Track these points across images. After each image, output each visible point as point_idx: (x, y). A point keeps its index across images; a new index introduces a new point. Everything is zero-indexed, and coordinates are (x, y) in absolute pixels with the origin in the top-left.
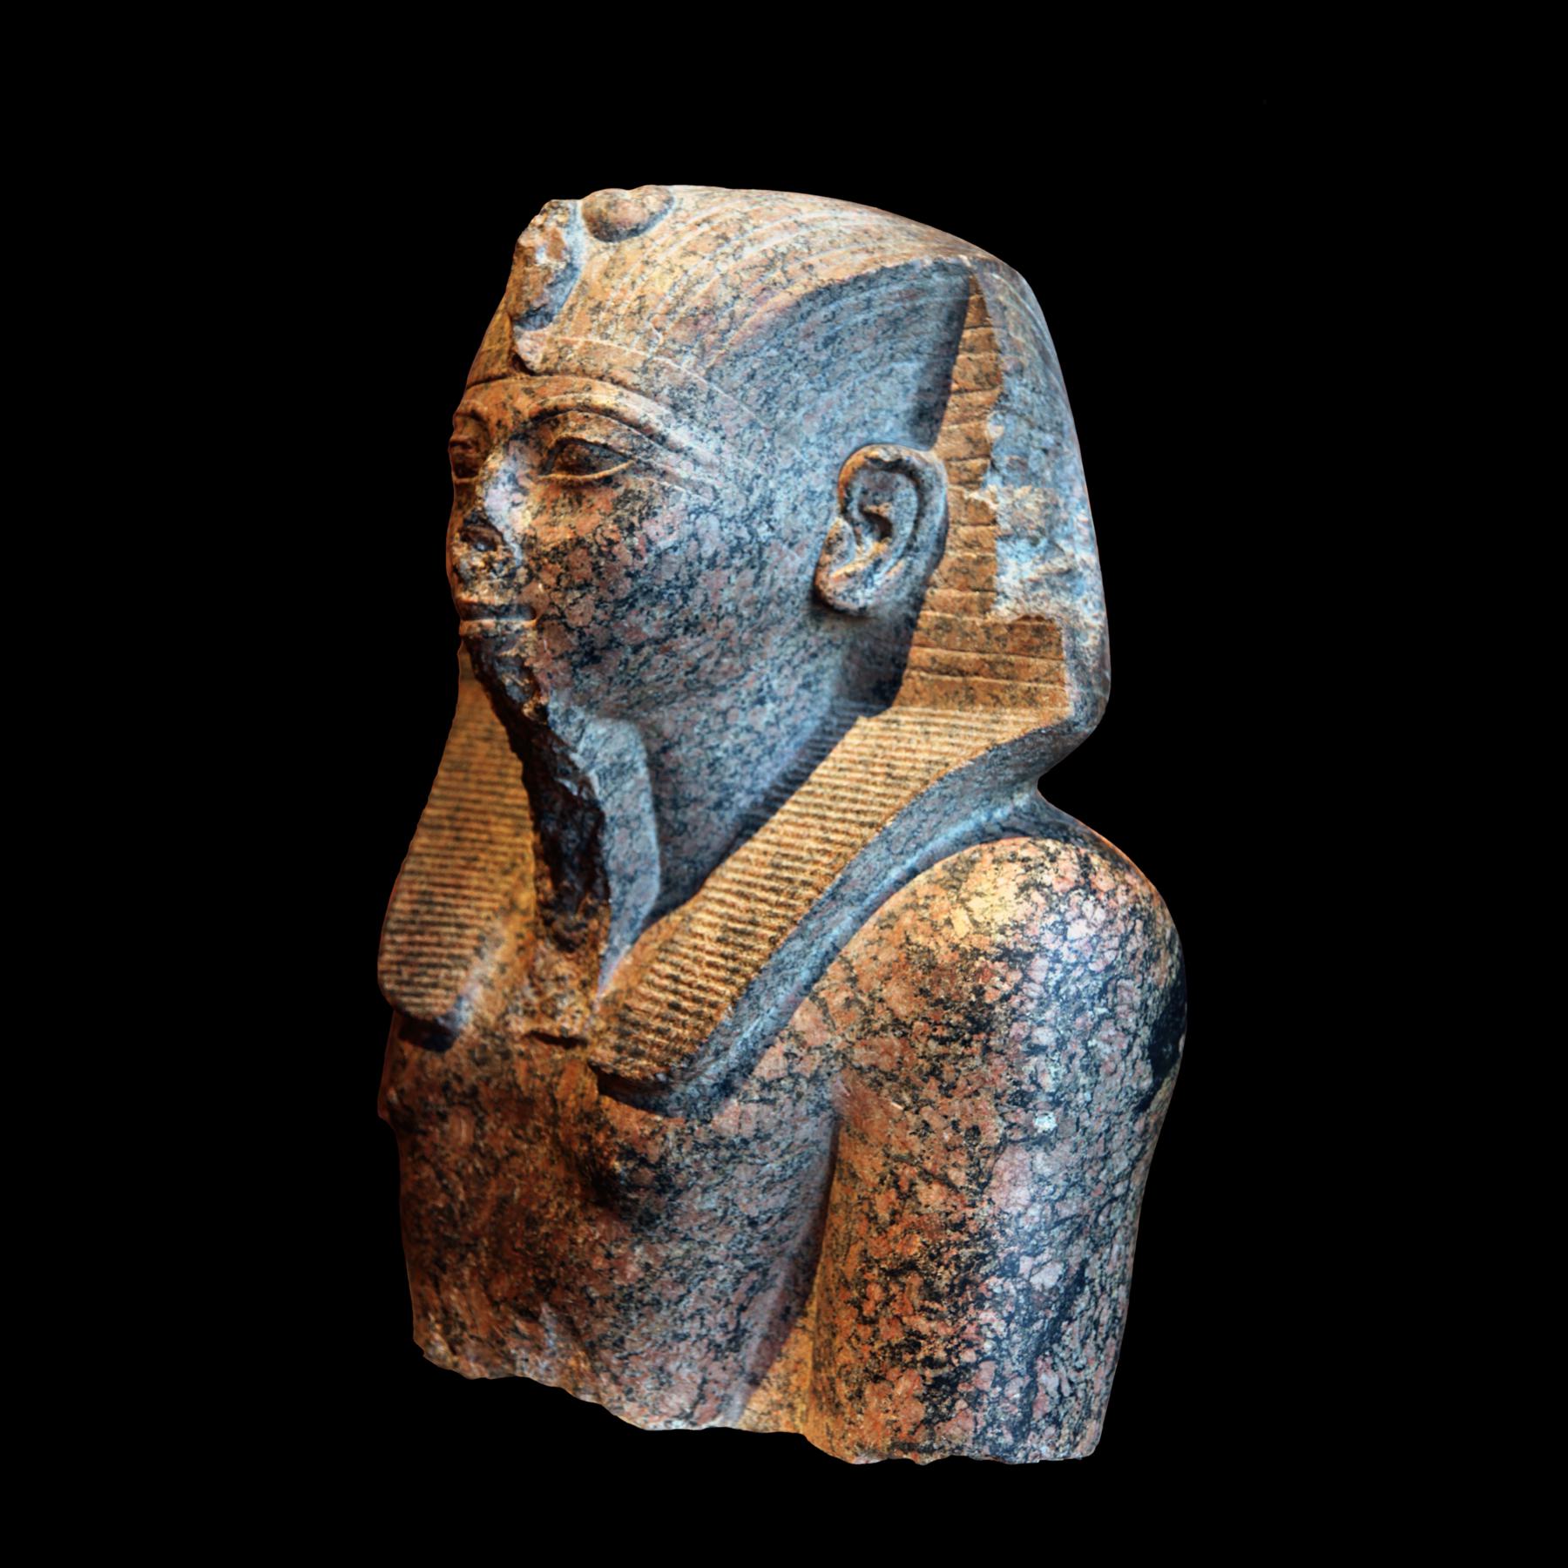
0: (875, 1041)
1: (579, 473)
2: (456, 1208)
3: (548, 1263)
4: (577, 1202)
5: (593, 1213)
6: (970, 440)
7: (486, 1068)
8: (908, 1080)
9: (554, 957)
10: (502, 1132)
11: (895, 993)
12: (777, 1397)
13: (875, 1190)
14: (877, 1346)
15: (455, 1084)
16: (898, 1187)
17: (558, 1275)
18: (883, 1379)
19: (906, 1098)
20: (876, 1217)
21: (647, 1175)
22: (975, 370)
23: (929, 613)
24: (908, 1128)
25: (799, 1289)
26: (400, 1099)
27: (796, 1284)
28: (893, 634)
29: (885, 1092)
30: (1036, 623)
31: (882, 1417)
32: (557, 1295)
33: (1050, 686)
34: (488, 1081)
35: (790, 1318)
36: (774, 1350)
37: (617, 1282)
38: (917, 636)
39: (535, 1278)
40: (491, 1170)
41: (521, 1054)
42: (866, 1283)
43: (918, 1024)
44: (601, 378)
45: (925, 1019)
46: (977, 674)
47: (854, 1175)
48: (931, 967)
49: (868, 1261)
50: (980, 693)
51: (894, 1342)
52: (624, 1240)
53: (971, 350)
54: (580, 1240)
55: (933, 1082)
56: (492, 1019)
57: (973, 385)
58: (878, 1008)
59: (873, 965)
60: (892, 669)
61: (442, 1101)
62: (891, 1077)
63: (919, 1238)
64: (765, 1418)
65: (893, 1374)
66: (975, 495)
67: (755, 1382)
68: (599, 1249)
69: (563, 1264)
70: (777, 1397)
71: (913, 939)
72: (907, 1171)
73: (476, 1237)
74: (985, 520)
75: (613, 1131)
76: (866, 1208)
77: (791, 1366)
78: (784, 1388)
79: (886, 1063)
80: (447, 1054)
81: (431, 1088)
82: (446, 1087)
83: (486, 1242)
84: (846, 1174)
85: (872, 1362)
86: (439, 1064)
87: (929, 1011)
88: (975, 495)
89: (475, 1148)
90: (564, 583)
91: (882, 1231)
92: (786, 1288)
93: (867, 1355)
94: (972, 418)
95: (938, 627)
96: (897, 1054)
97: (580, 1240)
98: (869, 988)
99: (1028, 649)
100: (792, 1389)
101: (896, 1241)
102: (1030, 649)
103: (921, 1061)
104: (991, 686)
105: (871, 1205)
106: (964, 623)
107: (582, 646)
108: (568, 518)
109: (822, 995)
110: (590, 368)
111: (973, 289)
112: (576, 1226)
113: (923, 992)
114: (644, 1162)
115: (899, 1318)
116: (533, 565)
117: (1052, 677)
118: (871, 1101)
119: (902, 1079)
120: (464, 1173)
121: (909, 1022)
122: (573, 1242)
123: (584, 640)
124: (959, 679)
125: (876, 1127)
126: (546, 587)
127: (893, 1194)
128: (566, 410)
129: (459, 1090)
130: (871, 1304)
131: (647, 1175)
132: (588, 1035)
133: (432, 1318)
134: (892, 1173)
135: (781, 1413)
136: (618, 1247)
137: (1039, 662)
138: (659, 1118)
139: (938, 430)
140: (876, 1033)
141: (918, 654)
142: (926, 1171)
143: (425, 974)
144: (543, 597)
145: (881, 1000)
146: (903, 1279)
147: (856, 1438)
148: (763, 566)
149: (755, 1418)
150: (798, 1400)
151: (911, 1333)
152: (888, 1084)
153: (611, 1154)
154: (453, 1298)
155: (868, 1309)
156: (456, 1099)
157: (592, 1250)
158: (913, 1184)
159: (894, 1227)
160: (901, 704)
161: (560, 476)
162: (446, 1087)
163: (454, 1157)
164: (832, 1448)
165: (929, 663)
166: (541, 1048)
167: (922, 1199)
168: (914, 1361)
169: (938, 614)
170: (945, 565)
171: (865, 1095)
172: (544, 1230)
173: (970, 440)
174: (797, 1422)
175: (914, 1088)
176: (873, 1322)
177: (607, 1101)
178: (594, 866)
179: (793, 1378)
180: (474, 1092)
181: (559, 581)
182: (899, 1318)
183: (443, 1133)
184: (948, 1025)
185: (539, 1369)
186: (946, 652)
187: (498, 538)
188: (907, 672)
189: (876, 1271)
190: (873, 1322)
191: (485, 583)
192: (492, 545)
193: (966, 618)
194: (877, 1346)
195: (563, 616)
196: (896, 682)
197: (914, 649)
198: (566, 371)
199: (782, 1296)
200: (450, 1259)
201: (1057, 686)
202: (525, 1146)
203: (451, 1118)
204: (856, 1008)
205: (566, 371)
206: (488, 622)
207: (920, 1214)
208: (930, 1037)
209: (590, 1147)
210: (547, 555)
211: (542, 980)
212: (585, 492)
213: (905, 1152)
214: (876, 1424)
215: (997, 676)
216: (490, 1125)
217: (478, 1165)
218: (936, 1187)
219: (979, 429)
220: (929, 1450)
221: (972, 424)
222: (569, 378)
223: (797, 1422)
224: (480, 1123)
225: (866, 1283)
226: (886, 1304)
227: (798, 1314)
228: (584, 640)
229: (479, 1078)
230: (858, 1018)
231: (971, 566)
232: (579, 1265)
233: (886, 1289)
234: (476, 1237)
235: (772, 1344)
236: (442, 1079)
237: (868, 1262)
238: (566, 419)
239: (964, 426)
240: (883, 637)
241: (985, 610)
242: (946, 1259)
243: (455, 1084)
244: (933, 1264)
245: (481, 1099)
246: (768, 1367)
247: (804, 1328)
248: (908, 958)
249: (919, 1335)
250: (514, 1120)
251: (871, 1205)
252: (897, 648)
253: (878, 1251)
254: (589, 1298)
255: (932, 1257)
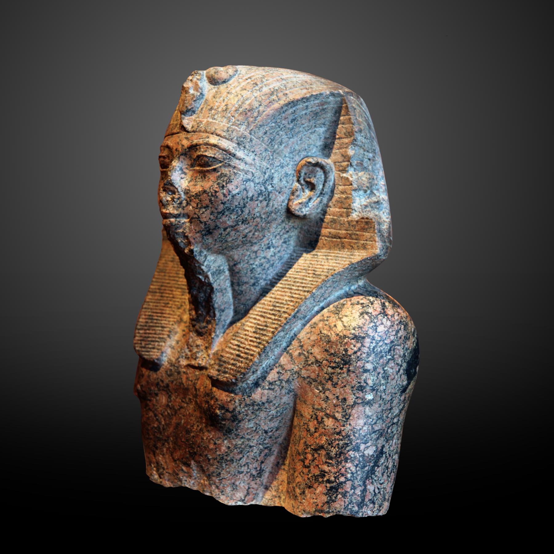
0: (309, 368)
1: (205, 167)
2: (161, 427)
3: (194, 446)
4: (204, 425)
5: (209, 428)
6: (343, 155)
7: (172, 377)
8: (321, 382)
9: (196, 338)
10: (177, 400)
11: (316, 351)
12: (274, 493)
13: (309, 420)
14: (310, 476)
15: (161, 383)
16: (317, 420)
17: (197, 451)
18: (312, 487)
19: (320, 388)
20: (309, 430)
21: (229, 415)
22: (344, 131)
23: (328, 217)
24: (321, 398)
25: (282, 456)
26: (141, 388)
27: (281, 454)
28: (315, 224)
29: (313, 386)
30: (366, 220)
31: (312, 501)
32: (197, 458)
33: (371, 243)
34: (172, 382)
35: (279, 466)
36: (273, 477)
37: (218, 453)
38: (324, 225)
39: (189, 451)
40: (173, 413)
41: (184, 372)
42: (306, 453)
43: (324, 362)
44: (212, 134)
45: (327, 360)
46: (345, 238)
47: (302, 415)
48: (329, 342)
49: (307, 445)
50: (346, 245)
51: (316, 474)
52: (220, 438)
53: (343, 124)
54: (205, 438)
55: (330, 382)
56: (174, 360)
57: (344, 136)
58: (310, 356)
59: (309, 341)
60: (315, 236)
61: (156, 389)
62: (315, 380)
63: (325, 438)
64: (270, 501)
65: (316, 485)
66: (344, 175)
67: (267, 488)
68: (212, 441)
69: (199, 447)
70: (274, 493)
71: (323, 332)
72: (320, 414)
73: (168, 437)
74: (348, 184)
75: (217, 400)
76: (306, 427)
77: (280, 483)
78: (277, 490)
79: (313, 376)
80: (158, 372)
81: (152, 384)
82: (158, 384)
83: (172, 439)
84: (299, 415)
85: (308, 481)
86: (155, 376)
87: (328, 357)
88: (344, 175)
89: (168, 406)
90: (199, 206)
91: (312, 435)
92: (278, 455)
93: (306, 479)
94: (344, 148)
95: (331, 222)
96: (317, 372)
97: (205, 438)
98: (307, 349)
99: (363, 229)
100: (280, 491)
101: (316, 438)
102: (364, 229)
103: (325, 375)
104: (350, 242)
105: (308, 426)
106: (341, 220)
107: (206, 228)
108: (201, 183)
109: (290, 351)
110: (208, 130)
111: (344, 102)
112: (203, 433)
113: (326, 350)
114: (227, 410)
115: (317, 466)
116: (188, 199)
117: (372, 239)
118: (308, 389)
119: (319, 381)
120: (164, 414)
121: (321, 361)
122: (202, 439)
123: (206, 226)
124: (339, 240)
125: (309, 398)
126: (193, 207)
127: (316, 422)
128: (200, 145)
129: (162, 385)
130: (308, 461)
131: (229, 415)
132: (208, 366)
133: (153, 466)
134: (315, 414)
135: (276, 499)
136: (218, 440)
137: (367, 234)
138: (233, 395)
139: (332, 152)
140: (309, 365)
141: (324, 231)
142: (327, 414)
143: (150, 344)
144: (192, 211)
145: (311, 353)
146: (319, 452)
147: (302, 508)
148: (269, 200)
149: (267, 501)
150: (282, 495)
151: (322, 471)
152: (314, 383)
153: (216, 408)
154: (160, 458)
155: (307, 463)
156: (161, 388)
157: (209, 442)
158: (322, 418)
159: (316, 434)
160: (318, 249)
161: (198, 168)
162: (158, 384)
163: (160, 409)
164: (294, 512)
165: (328, 234)
166: (191, 370)
167: (326, 424)
168: (323, 481)
169: (331, 217)
170: (334, 199)
171: (306, 387)
172: (192, 434)
173: (343, 155)
174: (282, 502)
175: (323, 384)
176: (308, 467)
177: (214, 389)
178: (210, 306)
179: (280, 487)
180: (168, 386)
181: (197, 205)
182: (317, 466)
183: (156, 400)
184: (335, 362)
185: (190, 484)
186: (334, 230)
187: (176, 190)
188: (320, 237)
189: (309, 449)
190: (308, 467)
191: (171, 206)
192: (174, 193)
193: (341, 218)
194: (310, 476)
195: (199, 218)
196: (317, 241)
197: (323, 229)
198: (200, 131)
199: (276, 458)
200: (159, 445)
201: (374, 242)
202: (186, 405)
203: (160, 395)
204: (302, 356)
205: (200, 131)
206: (173, 220)
207: (325, 429)
208: (329, 366)
209: (209, 405)
210: (193, 196)
211: (192, 346)
212: (207, 174)
213: (320, 407)
214: (309, 503)
215: (352, 239)
216: (173, 397)
217: (169, 412)
218: (331, 419)
219: (346, 152)
220: (328, 512)
221: (344, 150)
222: (201, 133)
223: (282, 502)
224: (170, 397)
225: (306, 453)
226: (313, 461)
227: (282, 464)
228: (206, 226)
229: (169, 381)
230: (303, 360)
231: (343, 200)
232: (204, 447)
233: (313, 456)
234: (168, 437)
235: (273, 475)
236: (156, 381)
237: (307, 446)
238: (200, 148)
239: (341, 150)
240: (312, 225)
241: (348, 216)
242: (334, 445)
243: (161, 383)
244: (330, 447)
245: (170, 388)
246: (271, 483)
247: (284, 469)
248: (321, 339)
249: (325, 472)
250: (182, 396)
251: (308, 426)
252: (317, 229)
253: (310, 442)
254: (208, 458)
255: (329, 444)
